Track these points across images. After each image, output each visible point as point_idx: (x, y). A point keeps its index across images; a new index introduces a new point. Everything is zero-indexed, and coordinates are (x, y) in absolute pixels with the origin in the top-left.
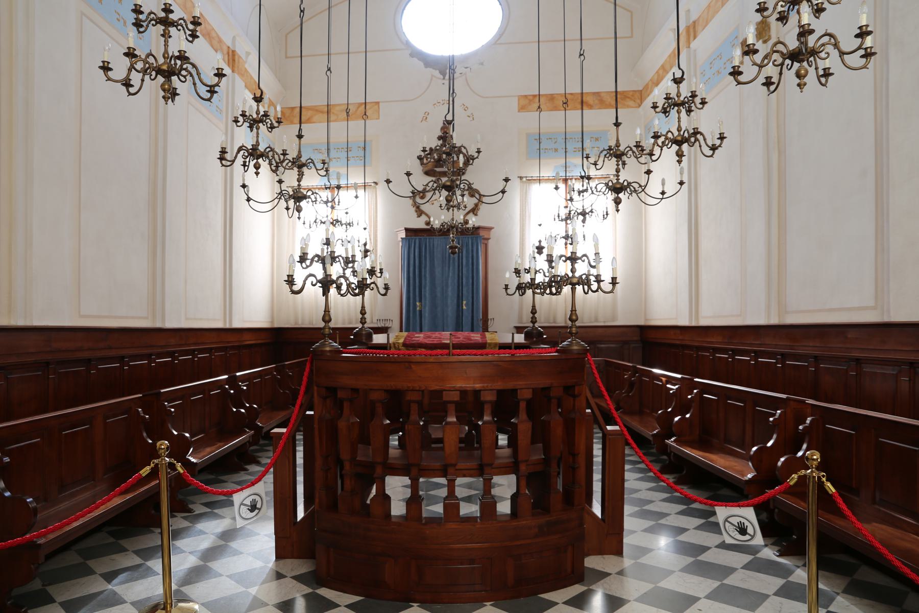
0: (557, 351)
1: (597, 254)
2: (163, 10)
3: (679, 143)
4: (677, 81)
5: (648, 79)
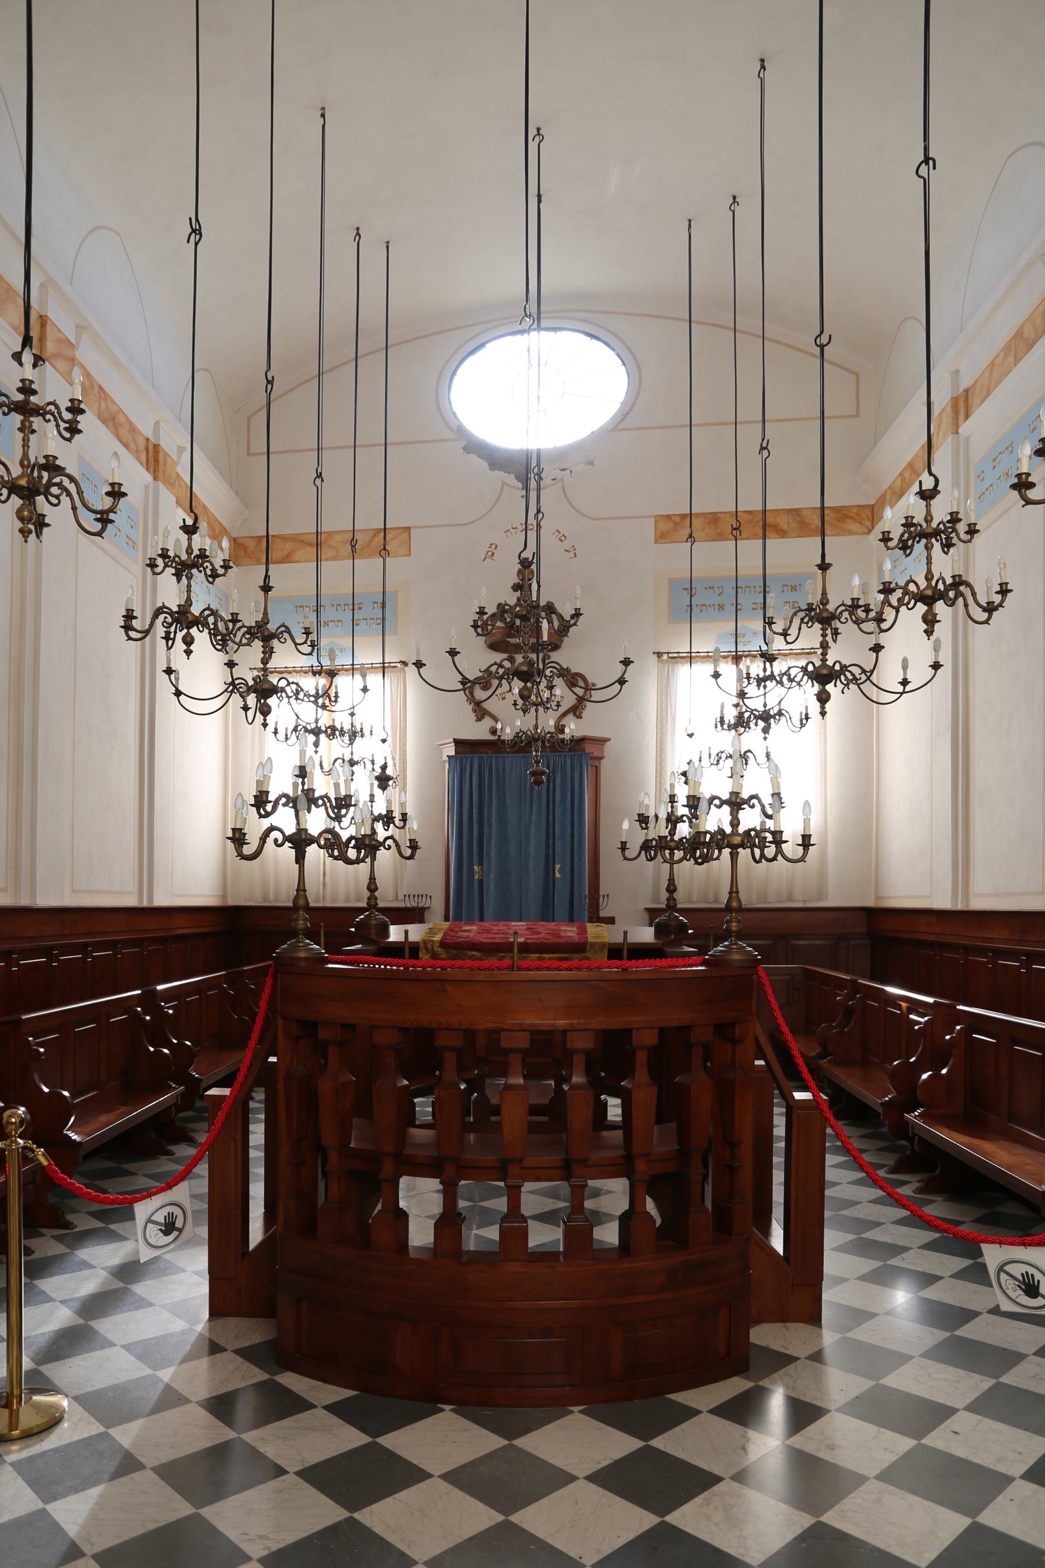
0: (704, 963)
1: (776, 795)
2: (19, 390)
3: (929, 599)
4: (927, 496)
5: (885, 485)
